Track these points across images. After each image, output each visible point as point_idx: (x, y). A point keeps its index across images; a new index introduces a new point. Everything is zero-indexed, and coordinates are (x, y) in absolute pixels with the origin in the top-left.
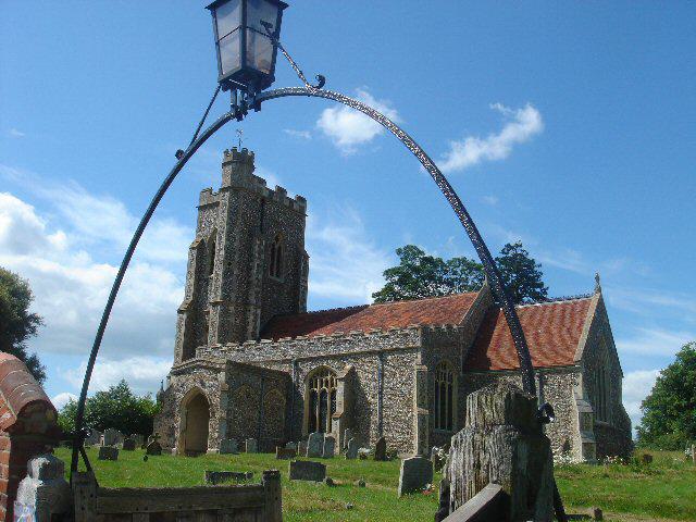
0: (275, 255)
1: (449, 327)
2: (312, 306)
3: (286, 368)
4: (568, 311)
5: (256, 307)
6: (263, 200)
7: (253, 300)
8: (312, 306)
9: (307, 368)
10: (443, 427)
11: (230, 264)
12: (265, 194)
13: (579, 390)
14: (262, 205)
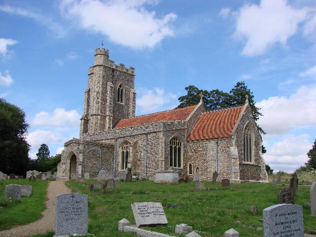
6: (113, 70)
10: (175, 166)
12: (114, 67)
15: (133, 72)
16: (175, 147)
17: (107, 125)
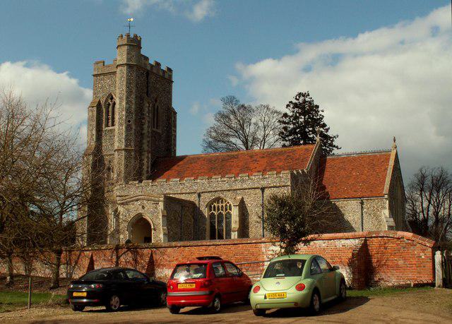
0: (155, 112)
1: (303, 171)
2: (179, 154)
3: (193, 198)
4: (110, 123)
5: (148, 152)
6: (148, 73)
7: (145, 147)
8: (179, 154)
9: (207, 198)
11: (129, 121)
12: (149, 68)
13: (387, 212)
14: (147, 76)
15: (170, 76)
16: (226, 205)
17: (146, 169)
